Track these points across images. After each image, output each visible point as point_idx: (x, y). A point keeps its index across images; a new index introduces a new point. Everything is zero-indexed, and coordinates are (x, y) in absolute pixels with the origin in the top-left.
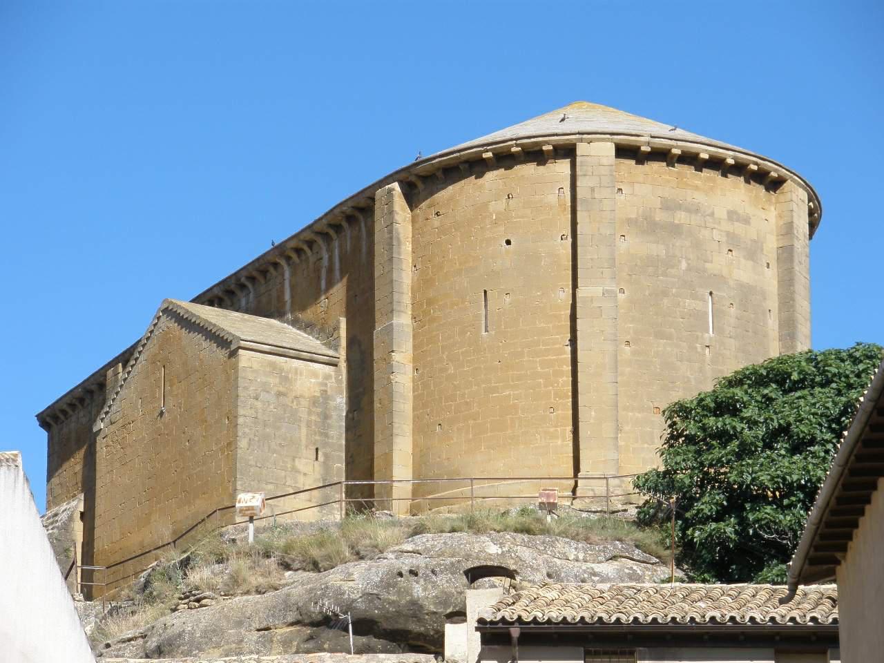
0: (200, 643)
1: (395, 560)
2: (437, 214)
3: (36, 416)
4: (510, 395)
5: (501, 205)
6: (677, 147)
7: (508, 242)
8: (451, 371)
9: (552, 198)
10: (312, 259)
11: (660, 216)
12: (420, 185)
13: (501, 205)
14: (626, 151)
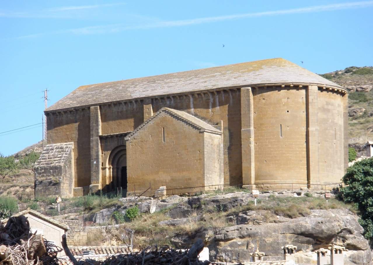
0: (264, 236)
1: (314, 218)
2: (264, 99)
3: (47, 113)
4: (289, 156)
5: (286, 100)
6: (331, 88)
7: (288, 111)
8: (270, 146)
9: (300, 100)
10: (204, 99)
11: (326, 107)
12: (257, 89)
13: (286, 100)
14: (321, 89)
